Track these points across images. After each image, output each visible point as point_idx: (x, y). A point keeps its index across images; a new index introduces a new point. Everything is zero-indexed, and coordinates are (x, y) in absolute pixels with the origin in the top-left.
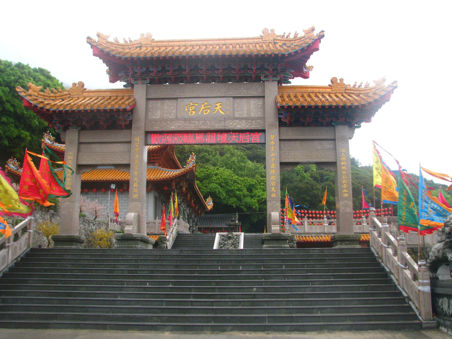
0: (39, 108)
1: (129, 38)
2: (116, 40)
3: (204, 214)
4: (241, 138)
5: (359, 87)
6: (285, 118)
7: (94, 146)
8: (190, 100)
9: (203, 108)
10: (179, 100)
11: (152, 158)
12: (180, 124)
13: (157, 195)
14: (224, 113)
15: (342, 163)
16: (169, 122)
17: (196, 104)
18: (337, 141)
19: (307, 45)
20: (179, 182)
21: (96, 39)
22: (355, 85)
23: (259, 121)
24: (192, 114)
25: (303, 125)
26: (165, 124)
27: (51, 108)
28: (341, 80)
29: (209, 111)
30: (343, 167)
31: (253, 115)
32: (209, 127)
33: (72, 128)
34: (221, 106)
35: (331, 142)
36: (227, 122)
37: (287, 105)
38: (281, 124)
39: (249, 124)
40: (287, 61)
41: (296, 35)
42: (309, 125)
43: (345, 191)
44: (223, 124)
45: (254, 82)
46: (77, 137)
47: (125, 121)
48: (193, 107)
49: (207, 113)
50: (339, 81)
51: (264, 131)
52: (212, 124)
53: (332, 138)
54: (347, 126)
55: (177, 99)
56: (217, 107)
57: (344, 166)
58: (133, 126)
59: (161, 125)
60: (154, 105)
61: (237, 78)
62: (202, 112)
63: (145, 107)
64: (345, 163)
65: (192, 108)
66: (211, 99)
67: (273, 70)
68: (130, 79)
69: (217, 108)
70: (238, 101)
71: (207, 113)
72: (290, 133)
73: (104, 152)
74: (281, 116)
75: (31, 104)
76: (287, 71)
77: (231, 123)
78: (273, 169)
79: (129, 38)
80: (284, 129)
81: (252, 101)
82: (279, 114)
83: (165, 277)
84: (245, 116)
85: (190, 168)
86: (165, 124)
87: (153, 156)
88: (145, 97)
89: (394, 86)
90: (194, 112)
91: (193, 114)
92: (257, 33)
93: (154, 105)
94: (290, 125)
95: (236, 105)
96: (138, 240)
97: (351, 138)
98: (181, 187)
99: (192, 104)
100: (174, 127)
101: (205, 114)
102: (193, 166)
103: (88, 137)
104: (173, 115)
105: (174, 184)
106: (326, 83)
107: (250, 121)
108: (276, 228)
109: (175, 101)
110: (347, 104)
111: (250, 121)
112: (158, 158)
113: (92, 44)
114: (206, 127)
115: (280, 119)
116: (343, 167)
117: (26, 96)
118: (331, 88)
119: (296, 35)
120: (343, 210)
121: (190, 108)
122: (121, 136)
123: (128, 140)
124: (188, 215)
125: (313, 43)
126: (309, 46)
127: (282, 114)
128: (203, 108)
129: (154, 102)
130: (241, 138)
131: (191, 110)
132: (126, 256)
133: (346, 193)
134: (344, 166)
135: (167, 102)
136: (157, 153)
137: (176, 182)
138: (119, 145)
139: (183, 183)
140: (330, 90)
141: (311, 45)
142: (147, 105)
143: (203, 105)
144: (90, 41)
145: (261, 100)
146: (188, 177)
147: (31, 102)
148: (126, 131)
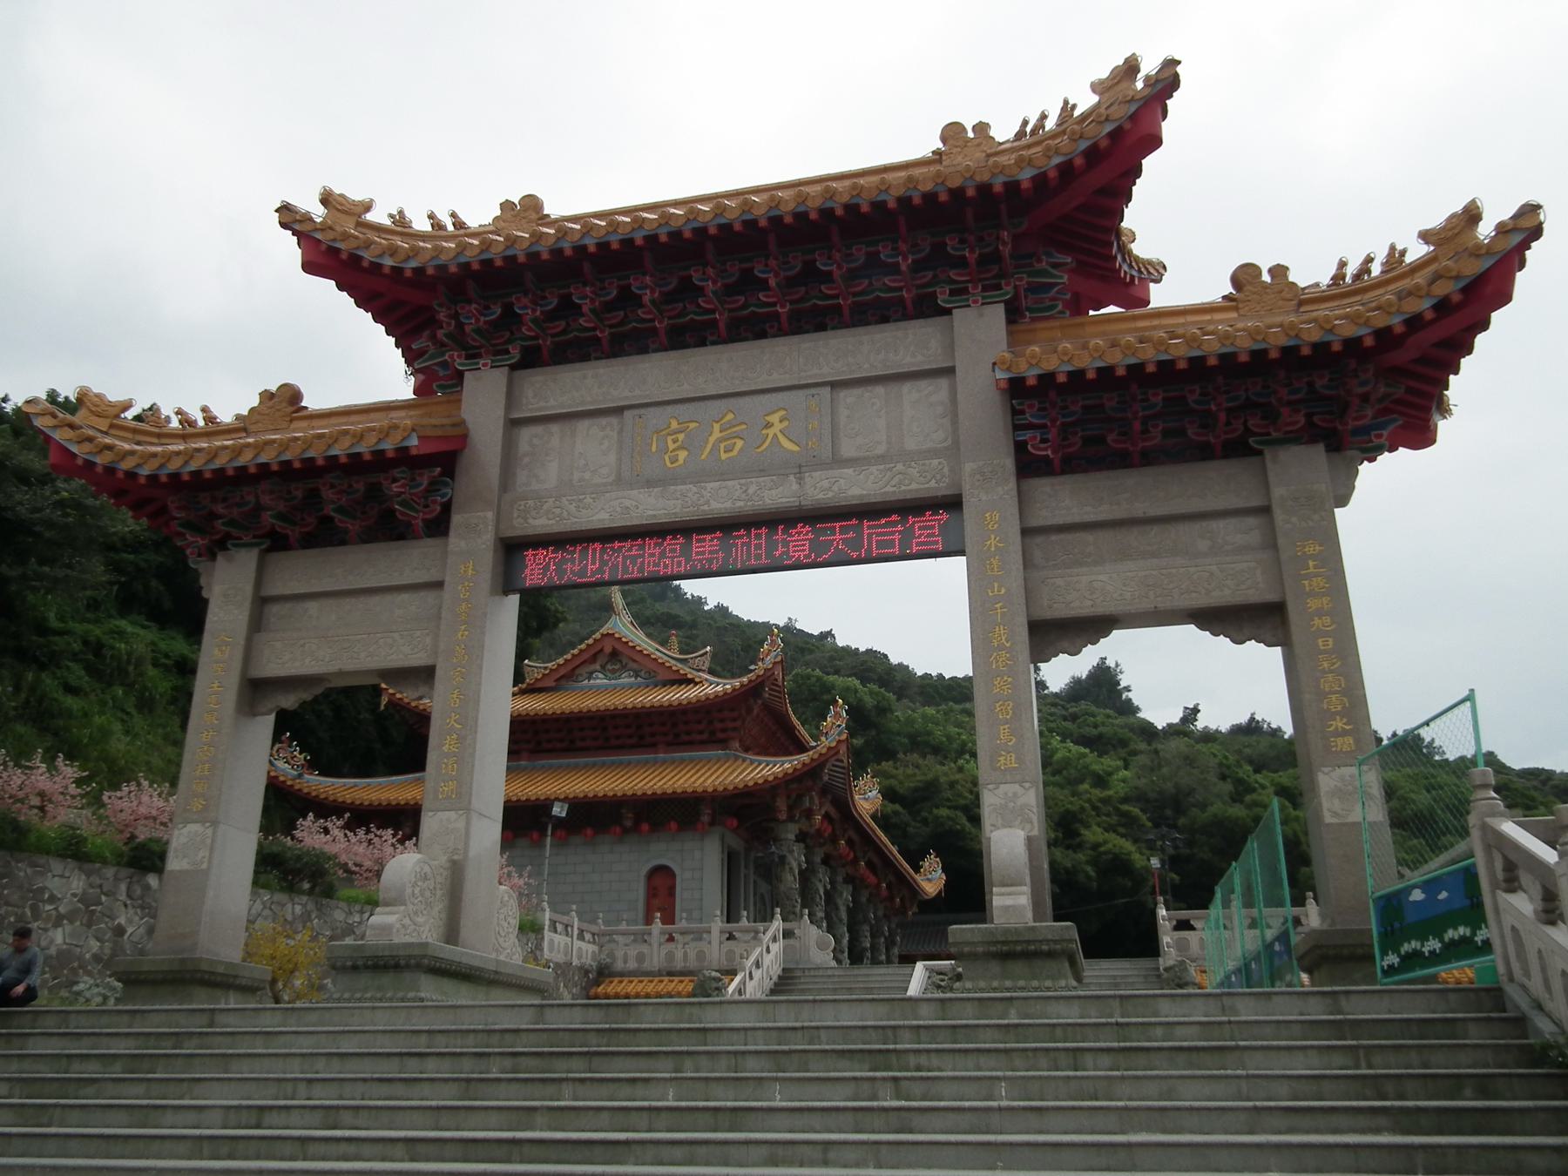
0: (120, 475)
1: (453, 215)
2: (400, 219)
3: (915, 909)
4: (870, 539)
5: (1357, 277)
6: (1044, 441)
7: (313, 607)
8: (669, 409)
9: (716, 434)
10: (627, 414)
11: (718, 725)
12: (627, 503)
13: (736, 843)
14: (796, 448)
15: (1313, 604)
16: (588, 500)
17: (693, 425)
18: (1279, 515)
19: (1108, 128)
20: (800, 797)
21: (318, 212)
22: (1338, 277)
23: (936, 462)
24: (674, 460)
25: (1121, 460)
26: (572, 508)
27: (139, 465)
28: (1279, 271)
29: (740, 443)
30: (1317, 621)
31: (911, 444)
32: (741, 504)
33: (236, 546)
34: (786, 423)
35: (1252, 521)
36: (807, 480)
37: (1036, 372)
38: (1028, 466)
39: (896, 480)
40: (1030, 217)
41: (1067, 108)
42: (1147, 459)
43: (1339, 724)
44: (795, 487)
45: (911, 318)
46: (253, 575)
47: (426, 506)
48: (681, 437)
49: (735, 453)
50: (1266, 278)
51: (953, 504)
52: (751, 491)
53: (1255, 502)
54: (1321, 447)
55: (619, 411)
56: (769, 425)
57: (1320, 613)
58: (456, 519)
59: (558, 511)
60: (535, 441)
61: (846, 312)
62: (715, 448)
63: (499, 448)
64: (1325, 600)
65: (675, 441)
66: (747, 399)
67: (984, 261)
68: (451, 357)
69: (771, 432)
70: (848, 397)
71: (735, 453)
72: (1064, 499)
73: (342, 620)
74: (1025, 436)
75: (74, 455)
76: (1039, 261)
77: (825, 484)
78: (1001, 648)
79: (453, 215)
80: (1043, 487)
81: (909, 391)
82: (1016, 428)
83: (367, 1150)
84: (881, 450)
85: (830, 749)
86: (572, 508)
87: (722, 721)
88: (501, 412)
89: (1526, 227)
90: (682, 455)
91: (681, 461)
92: (925, 143)
93: (535, 441)
94: (1069, 465)
95: (843, 413)
96: (366, 967)
97: (1343, 501)
98: (809, 814)
99: (674, 425)
100: (604, 516)
101: (724, 456)
102: (839, 742)
103: (298, 572)
104: (604, 471)
105: (782, 804)
106: (1217, 288)
107: (900, 467)
108: (1009, 901)
109: (614, 420)
110: (1305, 337)
111: (900, 467)
112: (739, 723)
113: (297, 227)
114: (728, 505)
115: (1020, 447)
116: (1317, 621)
117: (55, 427)
118: (1236, 309)
119: (1067, 108)
120: (1335, 814)
121: (670, 439)
122: (407, 561)
123: (433, 575)
124: (849, 911)
125: (1133, 118)
126: (1117, 135)
127: (1030, 426)
128: (716, 434)
129: (538, 429)
130: (870, 539)
131: (671, 446)
132: (282, 1039)
133: (1345, 733)
134: (1320, 613)
135: (583, 425)
136: (732, 710)
137: (788, 797)
138: (405, 596)
139: (811, 798)
140: (1234, 315)
141: (1128, 126)
142: (509, 446)
143: (717, 427)
144: (289, 217)
145: (943, 383)
146: (826, 778)
147: (74, 449)
148: (429, 541)
